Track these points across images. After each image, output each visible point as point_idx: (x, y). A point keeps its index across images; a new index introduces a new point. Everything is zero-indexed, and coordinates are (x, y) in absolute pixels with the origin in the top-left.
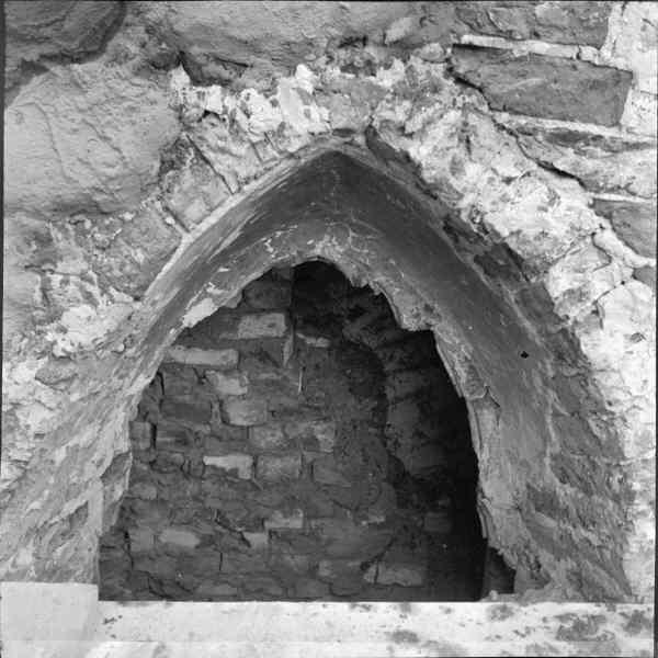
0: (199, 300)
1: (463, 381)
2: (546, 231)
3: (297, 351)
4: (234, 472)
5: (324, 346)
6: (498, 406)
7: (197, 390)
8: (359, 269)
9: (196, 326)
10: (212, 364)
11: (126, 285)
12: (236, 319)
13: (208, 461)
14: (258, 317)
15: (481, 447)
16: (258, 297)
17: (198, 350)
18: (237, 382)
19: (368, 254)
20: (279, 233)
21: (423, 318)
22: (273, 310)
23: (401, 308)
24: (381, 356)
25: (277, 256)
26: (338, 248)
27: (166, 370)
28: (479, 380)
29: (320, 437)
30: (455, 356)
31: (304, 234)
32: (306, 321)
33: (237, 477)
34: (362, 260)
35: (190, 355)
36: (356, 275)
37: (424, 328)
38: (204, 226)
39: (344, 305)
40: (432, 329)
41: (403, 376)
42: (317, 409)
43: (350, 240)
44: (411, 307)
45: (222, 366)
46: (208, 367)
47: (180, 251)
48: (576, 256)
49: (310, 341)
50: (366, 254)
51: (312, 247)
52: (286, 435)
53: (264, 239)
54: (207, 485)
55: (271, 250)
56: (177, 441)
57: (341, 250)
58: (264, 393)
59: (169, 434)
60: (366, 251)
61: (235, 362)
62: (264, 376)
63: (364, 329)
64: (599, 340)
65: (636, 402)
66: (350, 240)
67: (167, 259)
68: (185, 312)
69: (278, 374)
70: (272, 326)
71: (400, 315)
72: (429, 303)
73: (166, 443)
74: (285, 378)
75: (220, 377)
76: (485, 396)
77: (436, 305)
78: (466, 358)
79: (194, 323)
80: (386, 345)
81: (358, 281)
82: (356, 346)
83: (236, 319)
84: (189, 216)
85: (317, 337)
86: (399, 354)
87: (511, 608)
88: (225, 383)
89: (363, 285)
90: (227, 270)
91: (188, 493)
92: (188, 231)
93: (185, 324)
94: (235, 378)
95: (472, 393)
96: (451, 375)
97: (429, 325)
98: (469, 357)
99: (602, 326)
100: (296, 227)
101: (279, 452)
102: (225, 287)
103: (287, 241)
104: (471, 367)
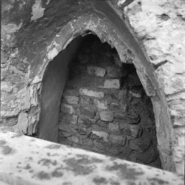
0: (52, 49)
4: (102, 138)
5: (139, 97)
8: (102, 35)
9: (53, 59)
10: (96, 96)
12: (103, 81)
13: (94, 132)
14: (111, 80)
16: (111, 72)
17: (91, 91)
18: (104, 104)
20: (75, 20)
22: (114, 78)
26: (94, 25)
29: (132, 130)
33: (103, 140)
34: (104, 31)
42: (131, 119)
43: (99, 22)
44: (123, 51)
45: (99, 98)
46: (94, 98)
49: (134, 95)
50: (105, 28)
51: (85, 26)
52: (120, 127)
53: (70, 23)
54: (95, 142)
55: (72, 27)
56: (84, 123)
58: (109, 108)
59: (82, 120)
61: (103, 96)
64: (139, 17)
65: (167, 58)
66: (99, 22)
68: (48, 53)
70: (115, 84)
72: (129, 48)
73: (80, 123)
74: (120, 105)
75: (98, 102)
78: (146, 75)
79: (52, 58)
83: (103, 81)
85: (136, 93)
87: (91, 167)
88: (100, 104)
89: (104, 42)
91: (89, 144)
94: (103, 103)
98: (147, 75)
99: (141, 10)
100: (80, 17)
101: (116, 133)
104: (148, 80)
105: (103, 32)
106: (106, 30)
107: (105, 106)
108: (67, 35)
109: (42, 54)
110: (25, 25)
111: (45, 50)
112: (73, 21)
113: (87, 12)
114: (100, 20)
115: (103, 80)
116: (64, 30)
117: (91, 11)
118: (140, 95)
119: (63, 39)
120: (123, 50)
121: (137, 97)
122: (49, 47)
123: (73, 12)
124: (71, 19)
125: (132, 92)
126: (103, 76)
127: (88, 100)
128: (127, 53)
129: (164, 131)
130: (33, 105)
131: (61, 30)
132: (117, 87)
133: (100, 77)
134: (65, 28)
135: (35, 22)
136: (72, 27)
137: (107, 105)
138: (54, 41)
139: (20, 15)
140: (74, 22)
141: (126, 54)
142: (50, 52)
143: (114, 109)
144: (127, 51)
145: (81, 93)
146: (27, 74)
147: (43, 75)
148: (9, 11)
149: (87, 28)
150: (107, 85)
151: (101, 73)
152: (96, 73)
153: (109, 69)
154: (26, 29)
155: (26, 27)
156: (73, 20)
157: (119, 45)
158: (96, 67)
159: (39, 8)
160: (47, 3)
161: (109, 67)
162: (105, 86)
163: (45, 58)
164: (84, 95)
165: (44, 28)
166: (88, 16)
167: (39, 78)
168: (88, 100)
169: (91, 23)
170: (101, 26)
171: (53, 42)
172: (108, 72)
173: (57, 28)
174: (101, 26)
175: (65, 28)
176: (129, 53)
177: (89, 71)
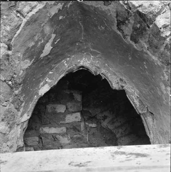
1: (138, 106)
2: (152, 4)
3: (86, 127)
5: (95, 126)
6: (152, 113)
7: (54, 142)
9: (44, 95)
11: (4, 40)
14: (72, 115)
15: (150, 133)
16: (71, 108)
17: (53, 128)
18: (66, 139)
19: (98, 63)
20: (68, 59)
21: (120, 84)
22: (75, 112)
23: (112, 81)
24: (115, 132)
25: (69, 67)
26: (88, 62)
27: (43, 136)
28: (143, 105)
30: (133, 97)
31: (77, 58)
34: (97, 65)
35: (50, 130)
36: (95, 71)
37: (121, 89)
38: (30, 14)
41: (123, 139)
45: (61, 133)
47: (22, 26)
48: (164, 14)
49: (90, 125)
53: (63, 61)
55: (66, 65)
57: (89, 63)
60: (97, 62)
62: (75, 136)
63: (108, 123)
66: (91, 59)
67: (18, 28)
69: (80, 135)
70: (76, 117)
71: (112, 84)
74: (83, 136)
75: (61, 137)
76: (147, 111)
77: (124, 78)
78: (137, 97)
79: (43, 94)
80: (116, 128)
81: (96, 73)
82: (107, 129)
84: (24, 11)
86: (120, 130)
88: (63, 139)
89: (98, 74)
92: (25, 18)
93: (40, 94)
94: (66, 137)
95: (142, 110)
96: (133, 105)
97: (122, 87)
98: (138, 96)
100: (73, 56)
102: (52, 79)
103: (71, 61)
104: (140, 100)
105: (96, 66)
107: (68, 140)
108: (61, 71)
111: (38, 87)
112: (66, 59)
113: (81, 51)
114: (93, 57)
115: (64, 115)
116: (58, 67)
117: (86, 50)
118: (95, 124)
120: (116, 79)
121: (93, 127)
122: (42, 84)
123: (69, 52)
124: (65, 58)
125: (88, 123)
126: (64, 112)
127: (50, 138)
129: (157, 140)
130: (19, 146)
131: (55, 68)
132: (78, 119)
134: (59, 65)
136: (66, 65)
137: (70, 138)
138: (47, 78)
139: (36, 52)
143: (77, 141)
144: (119, 79)
145: (41, 132)
146: (19, 112)
147: (31, 113)
148: (30, 48)
149: (81, 64)
150: (68, 120)
151: (61, 109)
153: (70, 104)
155: (37, 61)
158: (56, 105)
159: (50, 46)
160: (56, 43)
161: (69, 103)
162: (67, 121)
163: (36, 95)
164: (45, 134)
166: (81, 54)
167: (28, 116)
168: (50, 137)
169: (85, 60)
170: (94, 62)
171: (45, 79)
172: (69, 107)
174: (94, 62)
175: (59, 65)
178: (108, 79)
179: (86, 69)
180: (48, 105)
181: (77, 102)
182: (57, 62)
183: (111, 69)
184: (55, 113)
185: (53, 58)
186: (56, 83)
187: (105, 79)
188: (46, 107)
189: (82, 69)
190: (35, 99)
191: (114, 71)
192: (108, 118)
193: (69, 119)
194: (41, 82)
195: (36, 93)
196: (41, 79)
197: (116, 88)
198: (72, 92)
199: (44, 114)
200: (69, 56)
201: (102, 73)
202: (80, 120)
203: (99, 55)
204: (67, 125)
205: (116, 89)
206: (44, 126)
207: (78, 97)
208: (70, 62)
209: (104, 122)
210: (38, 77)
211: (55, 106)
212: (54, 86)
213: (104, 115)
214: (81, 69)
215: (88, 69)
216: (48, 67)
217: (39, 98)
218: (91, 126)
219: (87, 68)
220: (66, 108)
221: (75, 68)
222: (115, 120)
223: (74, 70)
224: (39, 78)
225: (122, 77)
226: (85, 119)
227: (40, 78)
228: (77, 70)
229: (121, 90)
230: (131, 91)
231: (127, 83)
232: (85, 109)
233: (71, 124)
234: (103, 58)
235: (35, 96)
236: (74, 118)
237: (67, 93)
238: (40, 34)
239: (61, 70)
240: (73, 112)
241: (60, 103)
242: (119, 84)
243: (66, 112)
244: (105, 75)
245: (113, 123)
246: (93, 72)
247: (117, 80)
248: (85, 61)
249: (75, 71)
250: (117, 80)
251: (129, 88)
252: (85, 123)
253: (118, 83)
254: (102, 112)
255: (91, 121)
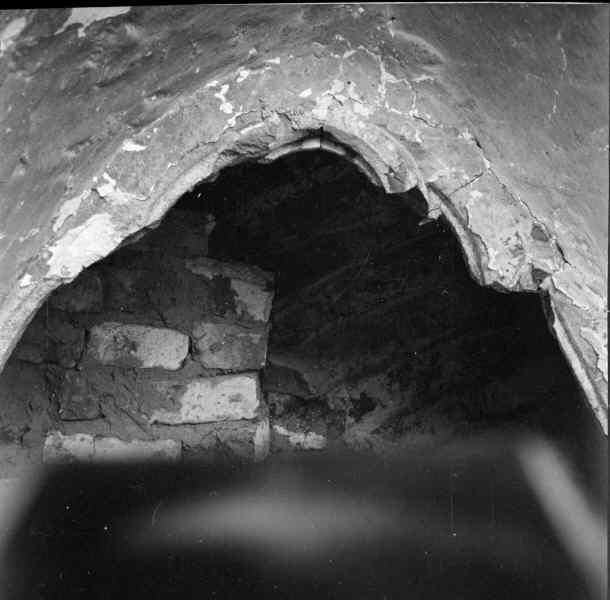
0: (81, 218)
12: (177, 387)
14: (214, 385)
20: (244, 73)
21: (529, 257)
22: (232, 373)
25: (242, 122)
26: (359, 107)
32: (290, 409)
34: (407, 135)
36: (395, 165)
37: (529, 285)
39: (345, 394)
40: (545, 284)
43: (382, 89)
44: (509, 232)
51: (311, 103)
53: (214, 83)
55: (227, 107)
63: (377, 431)
66: (382, 89)
68: (53, 239)
70: (236, 399)
72: (543, 219)
79: (74, 271)
90: (139, 148)
97: (538, 274)
100: (277, 61)
105: (402, 138)
106: (424, 132)
108: (191, 143)
109: (26, 241)
110: (30, 40)
114: (391, 79)
115: (176, 383)
116: (179, 115)
118: (321, 437)
119: (165, 165)
122: (70, 207)
126: (175, 365)
128: (527, 242)
132: (245, 410)
133: (160, 372)
134: (182, 108)
135: (78, 40)
136: (227, 107)
138: (106, 176)
140: (239, 80)
141: (520, 248)
142: (67, 238)
149: (321, 114)
150: (194, 407)
151: (164, 349)
152: (140, 353)
153: (208, 333)
154: (20, 74)
156: (235, 70)
157: (488, 205)
158: (142, 329)
161: (208, 327)
162: (187, 414)
165: (96, 88)
169: (344, 92)
171: (95, 179)
172: (203, 345)
173: (146, 101)
176: (540, 243)
177: (101, 349)
178: (465, 224)
179: (340, 152)
180: (99, 324)
181: (245, 322)
182: (177, 83)
183: (488, 164)
184: (128, 369)
185: (153, 46)
186: (158, 213)
187: (442, 218)
188: (87, 333)
189: (318, 151)
190: (22, 294)
191: (505, 180)
192: (378, 408)
193: (197, 403)
194: (71, 197)
195: (31, 260)
196: (69, 178)
197: (503, 278)
198: (228, 272)
199: (76, 368)
200: (253, 57)
201: (431, 186)
202: (251, 415)
203: (434, 69)
204: (188, 430)
205: (504, 283)
206: (68, 425)
207: (256, 302)
208: (254, 93)
209: (356, 427)
210: (44, 162)
211: (136, 331)
212: (145, 229)
213: (363, 395)
214: (314, 144)
215: (352, 152)
216: (121, 108)
217: (46, 289)
218: (298, 444)
219: (348, 149)
220: (190, 351)
221: (282, 134)
222: (407, 421)
223: (271, 145)
224: (55, 170)
225: (545, 220)
226: (274, 405)
227: (64, 166)
228: (286, 151)
229: (531, 294)
230: (589, 302)
231: (568, 256)
232: (278, 362)
233: (208, 428)
234: (456, 97)
235: (20, 277)
236: (224, 401)
237: (202, 276)
238: (190, 437)
239: (198, 137)
240: (222, 373)
241: (163, 320)
242: (522, 260)
243: (187, 367)
244: (446, 199)
245: (399, 432)
246: (381, 171)
247: (517, 235)
248: (342, 98)
249: (273, 156)
250: (517, 235)
251: (580, 287)
252: (271, 427)
253: (519, 250)
254: (352, 379)
255: (303, 417)
